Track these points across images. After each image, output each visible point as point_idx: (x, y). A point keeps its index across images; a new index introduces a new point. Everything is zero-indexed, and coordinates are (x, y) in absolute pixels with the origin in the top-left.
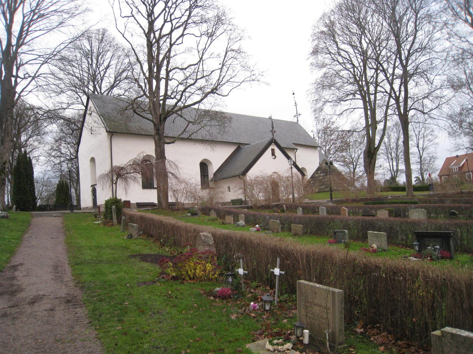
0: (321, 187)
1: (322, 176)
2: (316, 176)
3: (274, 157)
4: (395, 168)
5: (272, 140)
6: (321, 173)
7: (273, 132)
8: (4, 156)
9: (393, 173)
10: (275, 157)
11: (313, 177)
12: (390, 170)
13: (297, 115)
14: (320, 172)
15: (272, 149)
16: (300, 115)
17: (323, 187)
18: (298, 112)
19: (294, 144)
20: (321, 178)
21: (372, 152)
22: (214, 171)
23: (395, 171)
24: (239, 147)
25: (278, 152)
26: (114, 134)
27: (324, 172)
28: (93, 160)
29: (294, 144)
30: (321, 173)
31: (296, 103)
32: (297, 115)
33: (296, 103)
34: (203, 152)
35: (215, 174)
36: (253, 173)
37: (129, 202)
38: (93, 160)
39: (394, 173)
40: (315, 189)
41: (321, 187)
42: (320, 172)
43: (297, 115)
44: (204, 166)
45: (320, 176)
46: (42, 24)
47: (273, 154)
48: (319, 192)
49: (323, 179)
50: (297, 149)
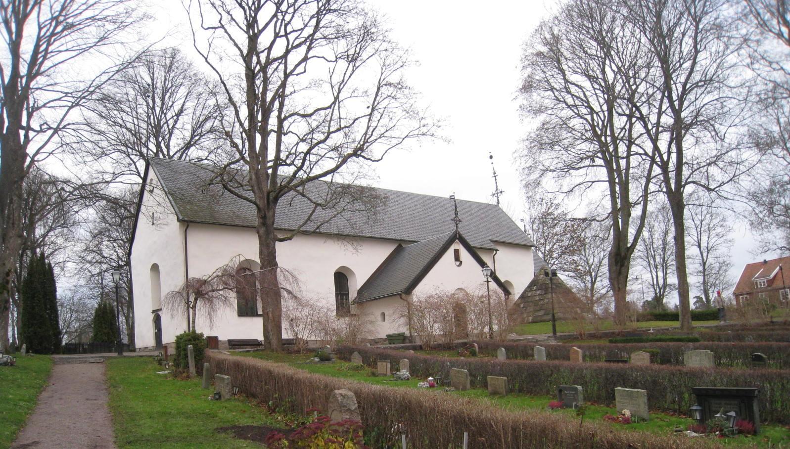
0: (537, 314)
1: (539, 295)
2: (530, 294)
3: (458, 263)
4: (661, 282)
5: (456, 235)
6: (537, 290)
7: (457, 221)
8: (6, 262)
9: (658, 290)
10: (461, 263)
11: (523, 297)
12: (653, 285)
13: (498, 193)
14: (535, 288)
15: (455, 250)
16: (501, 192)
17: (541, 313)
18: (499, 188)
19: (492, 241)
20: (537, 298)
21: (623, 254)
22: (359, 287)
23: (661, 286)
24: (400, 246)
25: (464, 254)
26: (191, 224)
27: (541, 289)
28: (155, 268)
29: (492, 241)
30: (537, 290)
31: (495, 173)
32: (498, 193)
33: (495, 173)
34: (340, 255)
35: (360, 292)
36: (422, 291)
37: (216, 338)
38: (155, 268)
39: (660, 289)
40: (528, 317)
41: (537, 314)
42: (535, 288)
43: (497, 193)
44: (341, 278)
45: (535, 296)
46: (69, 40)
47: (457, 258)
48: (533, 322)
49: (540, 300)
50: (497, 250)
